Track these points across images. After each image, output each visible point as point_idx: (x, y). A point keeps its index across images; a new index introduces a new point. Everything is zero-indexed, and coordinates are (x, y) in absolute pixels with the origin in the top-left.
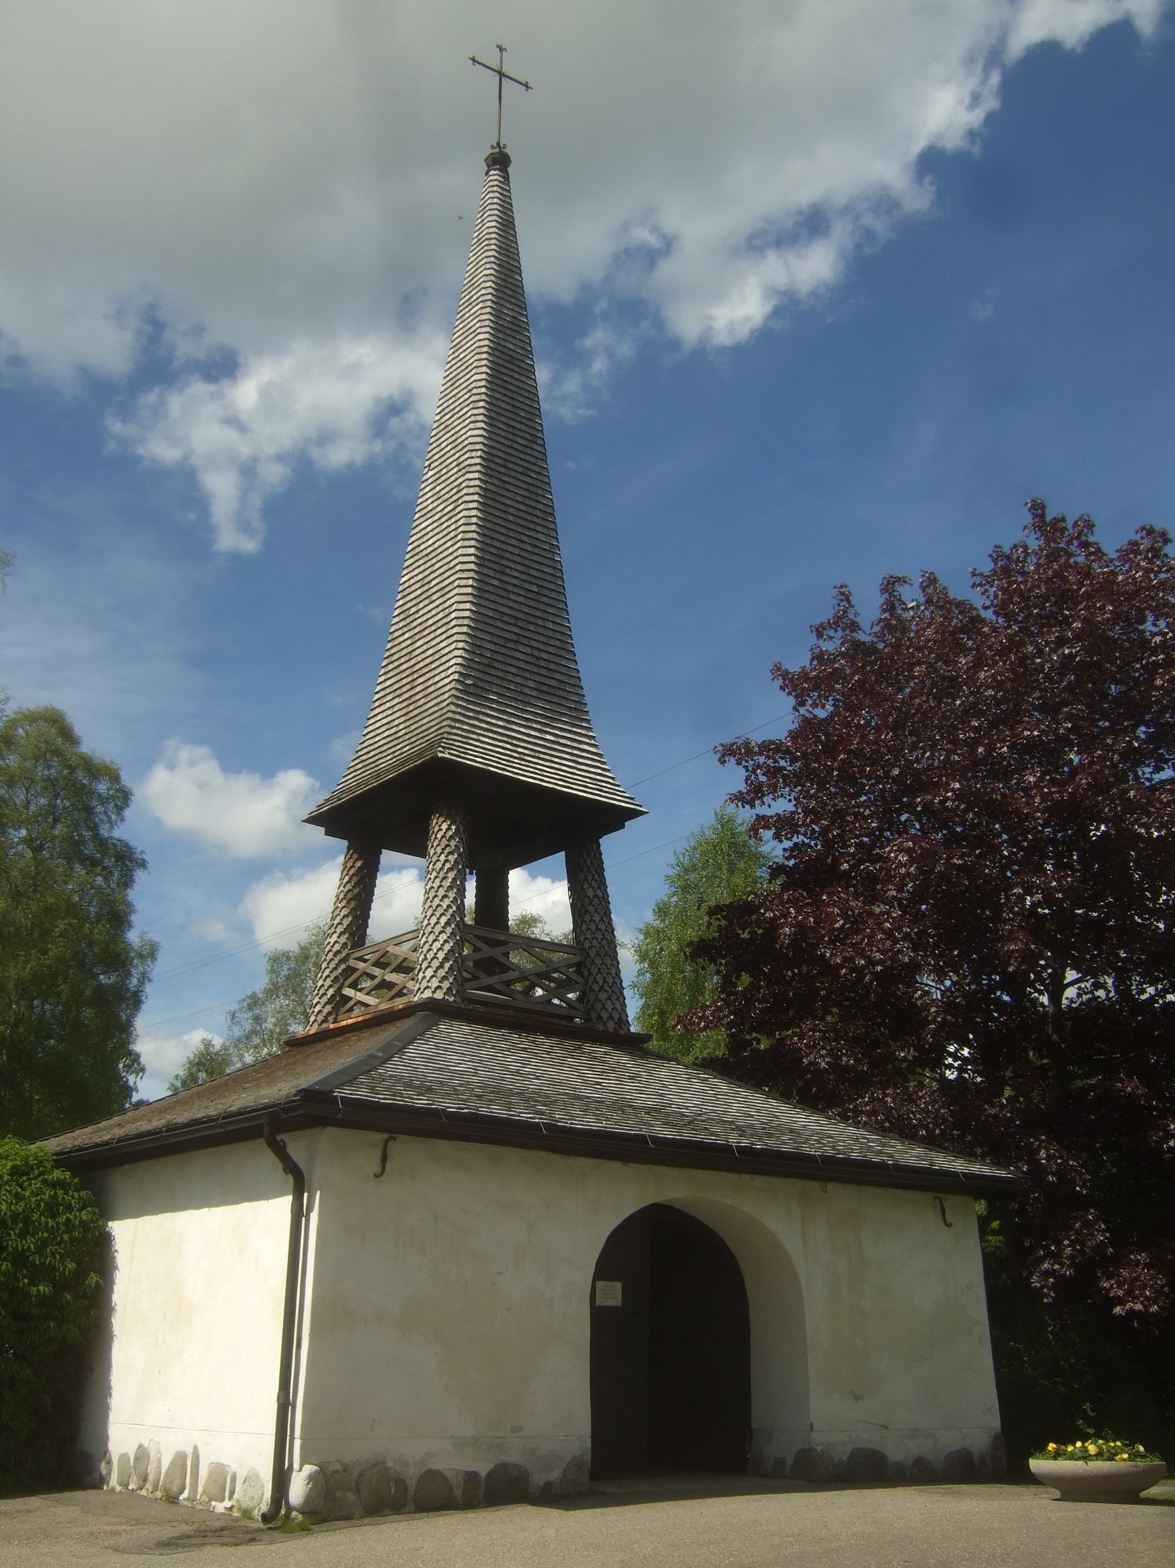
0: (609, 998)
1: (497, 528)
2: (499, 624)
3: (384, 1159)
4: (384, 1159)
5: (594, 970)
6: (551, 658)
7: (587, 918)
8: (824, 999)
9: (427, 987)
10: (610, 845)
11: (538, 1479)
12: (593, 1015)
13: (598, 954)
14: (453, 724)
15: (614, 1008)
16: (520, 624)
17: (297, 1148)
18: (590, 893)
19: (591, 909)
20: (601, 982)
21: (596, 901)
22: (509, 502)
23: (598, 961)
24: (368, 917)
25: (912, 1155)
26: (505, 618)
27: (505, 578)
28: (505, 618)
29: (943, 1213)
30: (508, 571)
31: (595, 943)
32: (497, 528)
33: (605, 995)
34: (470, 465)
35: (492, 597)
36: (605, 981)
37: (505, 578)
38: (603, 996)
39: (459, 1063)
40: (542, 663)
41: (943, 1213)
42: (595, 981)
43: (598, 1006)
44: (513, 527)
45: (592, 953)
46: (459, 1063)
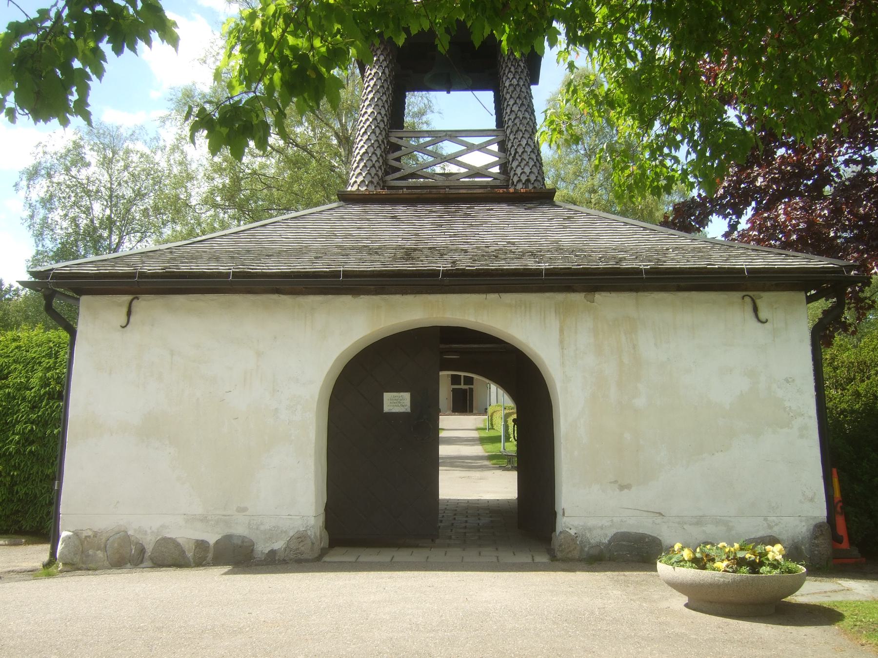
3: (129, 313)
4: (129, 313)
29: (755, 310)
41: (755, 310)
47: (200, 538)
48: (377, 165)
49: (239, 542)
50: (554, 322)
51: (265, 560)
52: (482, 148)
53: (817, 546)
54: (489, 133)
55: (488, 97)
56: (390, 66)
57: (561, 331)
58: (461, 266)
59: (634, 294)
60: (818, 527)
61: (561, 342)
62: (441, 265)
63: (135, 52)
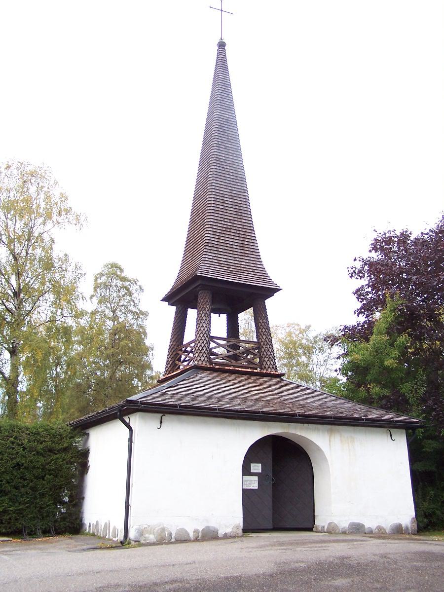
0: (269, 360)
1: (221, 186)
2: (223, 223)
3: (161, 423)
4: (161, 423)
5: (263, 350)
6: (244, 233)
7: (260, 331)
8: (261, 369)
9: (196, 360)
10: (269, 302)
11: (221, 532)
12: (263, 367)
13: (264, 344)
14: (204, 262)
15: (270, 364)
16: (232, 221)
17: (392, 430)
18: (261, 321)
19: (262, 327)
20: (265, 354)
21: (263, 324)
22: (227, 176)
23: (264, 347)
24: (185, 329)
25: (375, 414)
26: (226, 220)
27: (225, 205)
28: (226, 220)
29: (391, 436)
30: (226, 202)
31: (263, 340)
32: (221, 186)
33: (267, 359)
34: (211, 163)
35: (220, 213)
36: (267, 354)
37: (225, 205)
38: (266, 359)
39: (203, 388)
40: (241, 236)
41: (391, 436)
42: (263, 354)
43: (265, 363)
44: (229, 185)
45: (262, 344)
46: (203, 388)
47: (196, 528)
48: (206, 352)
49: (213, 529)
50: (327, 437)
51: (224, 537)
52: (222, 346)
53: (414, 526)
54: (253, 343)
55: (196, 311)
56: (363, 352)
57: (330, 441)
58: (370, 417)
59: (353, 427)
60: (413, 519)
61: (330, 445)
62: (349, 415)
63: (162, 300)
